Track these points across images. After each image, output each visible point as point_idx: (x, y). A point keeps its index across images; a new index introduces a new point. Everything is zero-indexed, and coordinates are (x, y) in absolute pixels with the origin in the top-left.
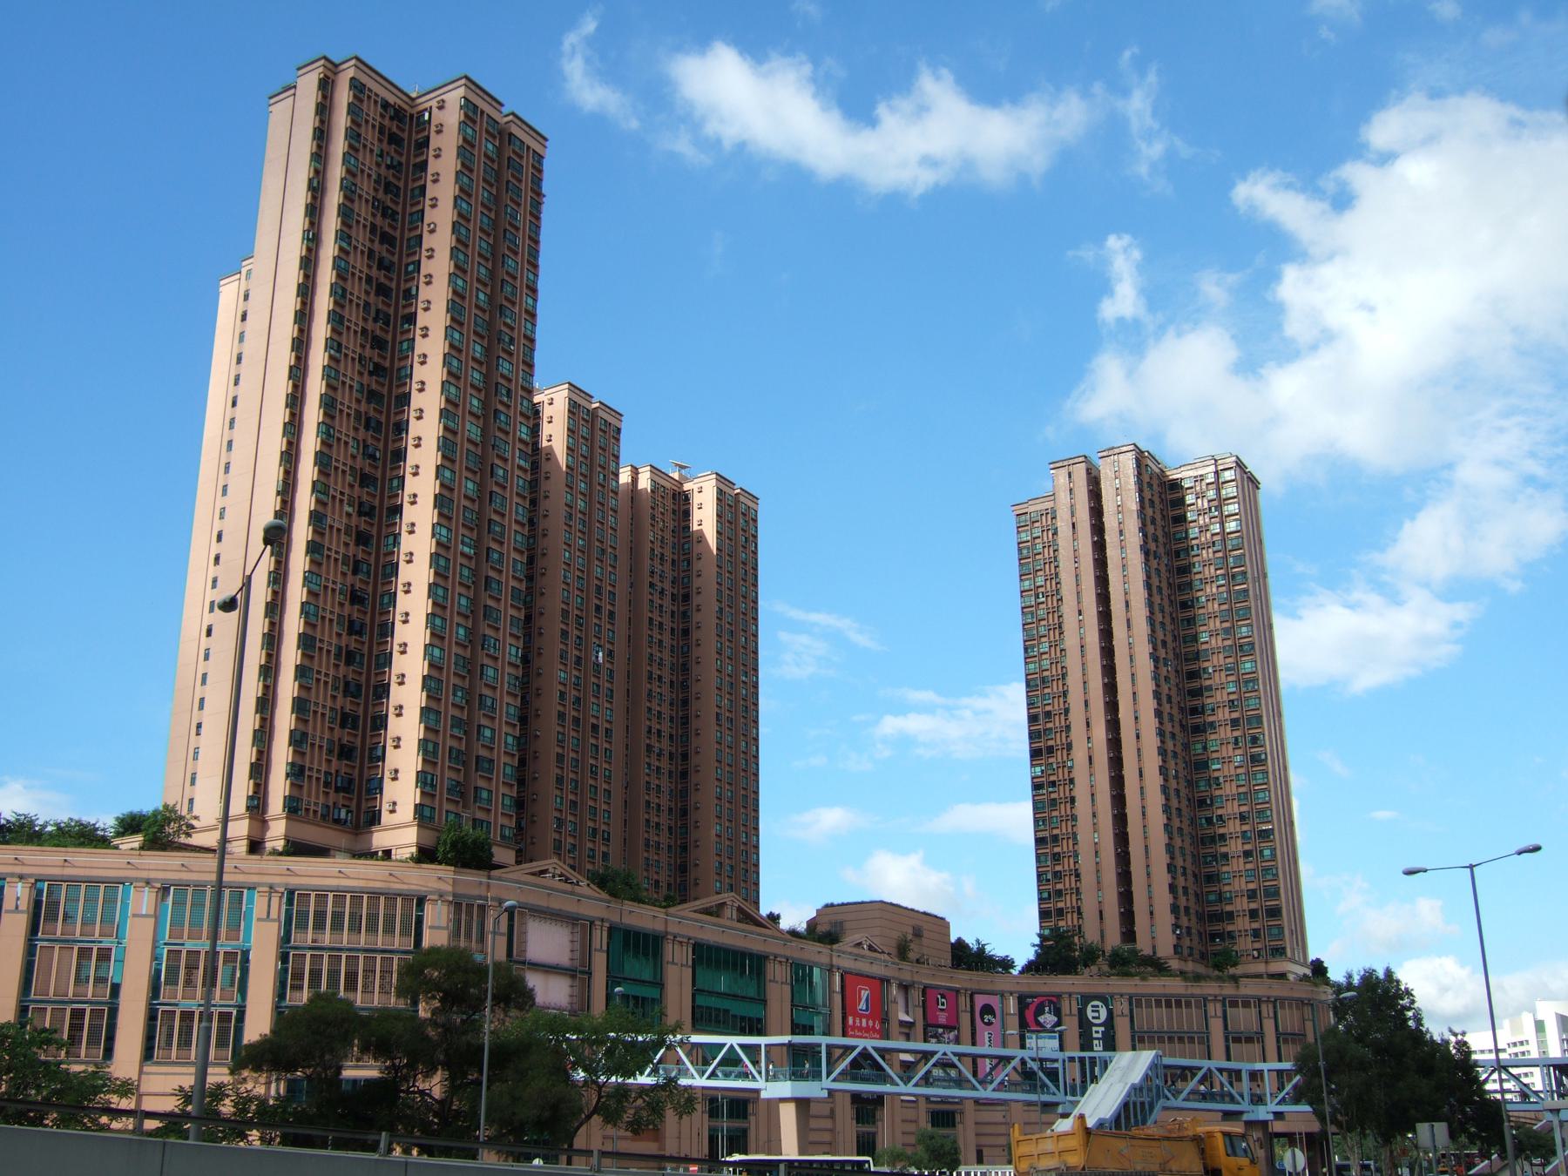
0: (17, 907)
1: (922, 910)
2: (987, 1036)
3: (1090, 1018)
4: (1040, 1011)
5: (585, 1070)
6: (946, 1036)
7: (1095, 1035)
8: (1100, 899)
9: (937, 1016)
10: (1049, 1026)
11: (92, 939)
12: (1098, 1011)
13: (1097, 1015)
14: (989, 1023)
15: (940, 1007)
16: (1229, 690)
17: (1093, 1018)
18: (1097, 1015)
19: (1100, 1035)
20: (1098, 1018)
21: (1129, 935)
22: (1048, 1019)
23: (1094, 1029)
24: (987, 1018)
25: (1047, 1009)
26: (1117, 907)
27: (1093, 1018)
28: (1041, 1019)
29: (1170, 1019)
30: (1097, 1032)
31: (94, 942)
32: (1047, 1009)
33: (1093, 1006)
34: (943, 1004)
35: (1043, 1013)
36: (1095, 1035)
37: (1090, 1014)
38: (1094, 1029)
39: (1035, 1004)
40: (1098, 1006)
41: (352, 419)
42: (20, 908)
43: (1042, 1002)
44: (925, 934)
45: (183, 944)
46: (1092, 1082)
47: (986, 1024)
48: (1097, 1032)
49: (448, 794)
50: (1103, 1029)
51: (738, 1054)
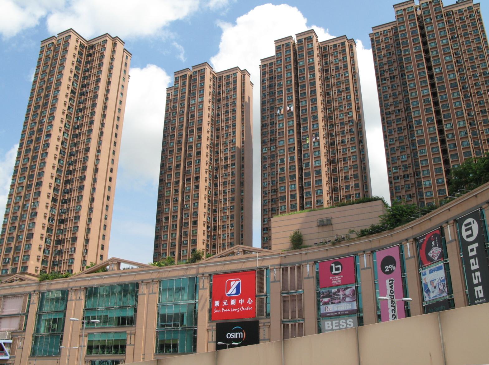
2: (388, 282)
3: (465, 238)
4: (429, 248)
6: (341, 293)
9: (331, 281)
10: (436, 258)
11: (287, 320)
14: (391, 271)
15: (334, 272)
16: (403, 160)
19: (475, 253)
20: (471, 235)
22: (436, 251)
24: (387, 268)
25: (433, 243)
30: (472, 250)
31: (289, 321)
32: (433, 243)
33: (466, 225)
37: (465, 234)
39: (425, 243)
40: (470, 224)
41: (84, 324)
44: (333, 221)
46: (292, 337)
48: (472, 250)
49: (465, 156)
50: (476, 245)
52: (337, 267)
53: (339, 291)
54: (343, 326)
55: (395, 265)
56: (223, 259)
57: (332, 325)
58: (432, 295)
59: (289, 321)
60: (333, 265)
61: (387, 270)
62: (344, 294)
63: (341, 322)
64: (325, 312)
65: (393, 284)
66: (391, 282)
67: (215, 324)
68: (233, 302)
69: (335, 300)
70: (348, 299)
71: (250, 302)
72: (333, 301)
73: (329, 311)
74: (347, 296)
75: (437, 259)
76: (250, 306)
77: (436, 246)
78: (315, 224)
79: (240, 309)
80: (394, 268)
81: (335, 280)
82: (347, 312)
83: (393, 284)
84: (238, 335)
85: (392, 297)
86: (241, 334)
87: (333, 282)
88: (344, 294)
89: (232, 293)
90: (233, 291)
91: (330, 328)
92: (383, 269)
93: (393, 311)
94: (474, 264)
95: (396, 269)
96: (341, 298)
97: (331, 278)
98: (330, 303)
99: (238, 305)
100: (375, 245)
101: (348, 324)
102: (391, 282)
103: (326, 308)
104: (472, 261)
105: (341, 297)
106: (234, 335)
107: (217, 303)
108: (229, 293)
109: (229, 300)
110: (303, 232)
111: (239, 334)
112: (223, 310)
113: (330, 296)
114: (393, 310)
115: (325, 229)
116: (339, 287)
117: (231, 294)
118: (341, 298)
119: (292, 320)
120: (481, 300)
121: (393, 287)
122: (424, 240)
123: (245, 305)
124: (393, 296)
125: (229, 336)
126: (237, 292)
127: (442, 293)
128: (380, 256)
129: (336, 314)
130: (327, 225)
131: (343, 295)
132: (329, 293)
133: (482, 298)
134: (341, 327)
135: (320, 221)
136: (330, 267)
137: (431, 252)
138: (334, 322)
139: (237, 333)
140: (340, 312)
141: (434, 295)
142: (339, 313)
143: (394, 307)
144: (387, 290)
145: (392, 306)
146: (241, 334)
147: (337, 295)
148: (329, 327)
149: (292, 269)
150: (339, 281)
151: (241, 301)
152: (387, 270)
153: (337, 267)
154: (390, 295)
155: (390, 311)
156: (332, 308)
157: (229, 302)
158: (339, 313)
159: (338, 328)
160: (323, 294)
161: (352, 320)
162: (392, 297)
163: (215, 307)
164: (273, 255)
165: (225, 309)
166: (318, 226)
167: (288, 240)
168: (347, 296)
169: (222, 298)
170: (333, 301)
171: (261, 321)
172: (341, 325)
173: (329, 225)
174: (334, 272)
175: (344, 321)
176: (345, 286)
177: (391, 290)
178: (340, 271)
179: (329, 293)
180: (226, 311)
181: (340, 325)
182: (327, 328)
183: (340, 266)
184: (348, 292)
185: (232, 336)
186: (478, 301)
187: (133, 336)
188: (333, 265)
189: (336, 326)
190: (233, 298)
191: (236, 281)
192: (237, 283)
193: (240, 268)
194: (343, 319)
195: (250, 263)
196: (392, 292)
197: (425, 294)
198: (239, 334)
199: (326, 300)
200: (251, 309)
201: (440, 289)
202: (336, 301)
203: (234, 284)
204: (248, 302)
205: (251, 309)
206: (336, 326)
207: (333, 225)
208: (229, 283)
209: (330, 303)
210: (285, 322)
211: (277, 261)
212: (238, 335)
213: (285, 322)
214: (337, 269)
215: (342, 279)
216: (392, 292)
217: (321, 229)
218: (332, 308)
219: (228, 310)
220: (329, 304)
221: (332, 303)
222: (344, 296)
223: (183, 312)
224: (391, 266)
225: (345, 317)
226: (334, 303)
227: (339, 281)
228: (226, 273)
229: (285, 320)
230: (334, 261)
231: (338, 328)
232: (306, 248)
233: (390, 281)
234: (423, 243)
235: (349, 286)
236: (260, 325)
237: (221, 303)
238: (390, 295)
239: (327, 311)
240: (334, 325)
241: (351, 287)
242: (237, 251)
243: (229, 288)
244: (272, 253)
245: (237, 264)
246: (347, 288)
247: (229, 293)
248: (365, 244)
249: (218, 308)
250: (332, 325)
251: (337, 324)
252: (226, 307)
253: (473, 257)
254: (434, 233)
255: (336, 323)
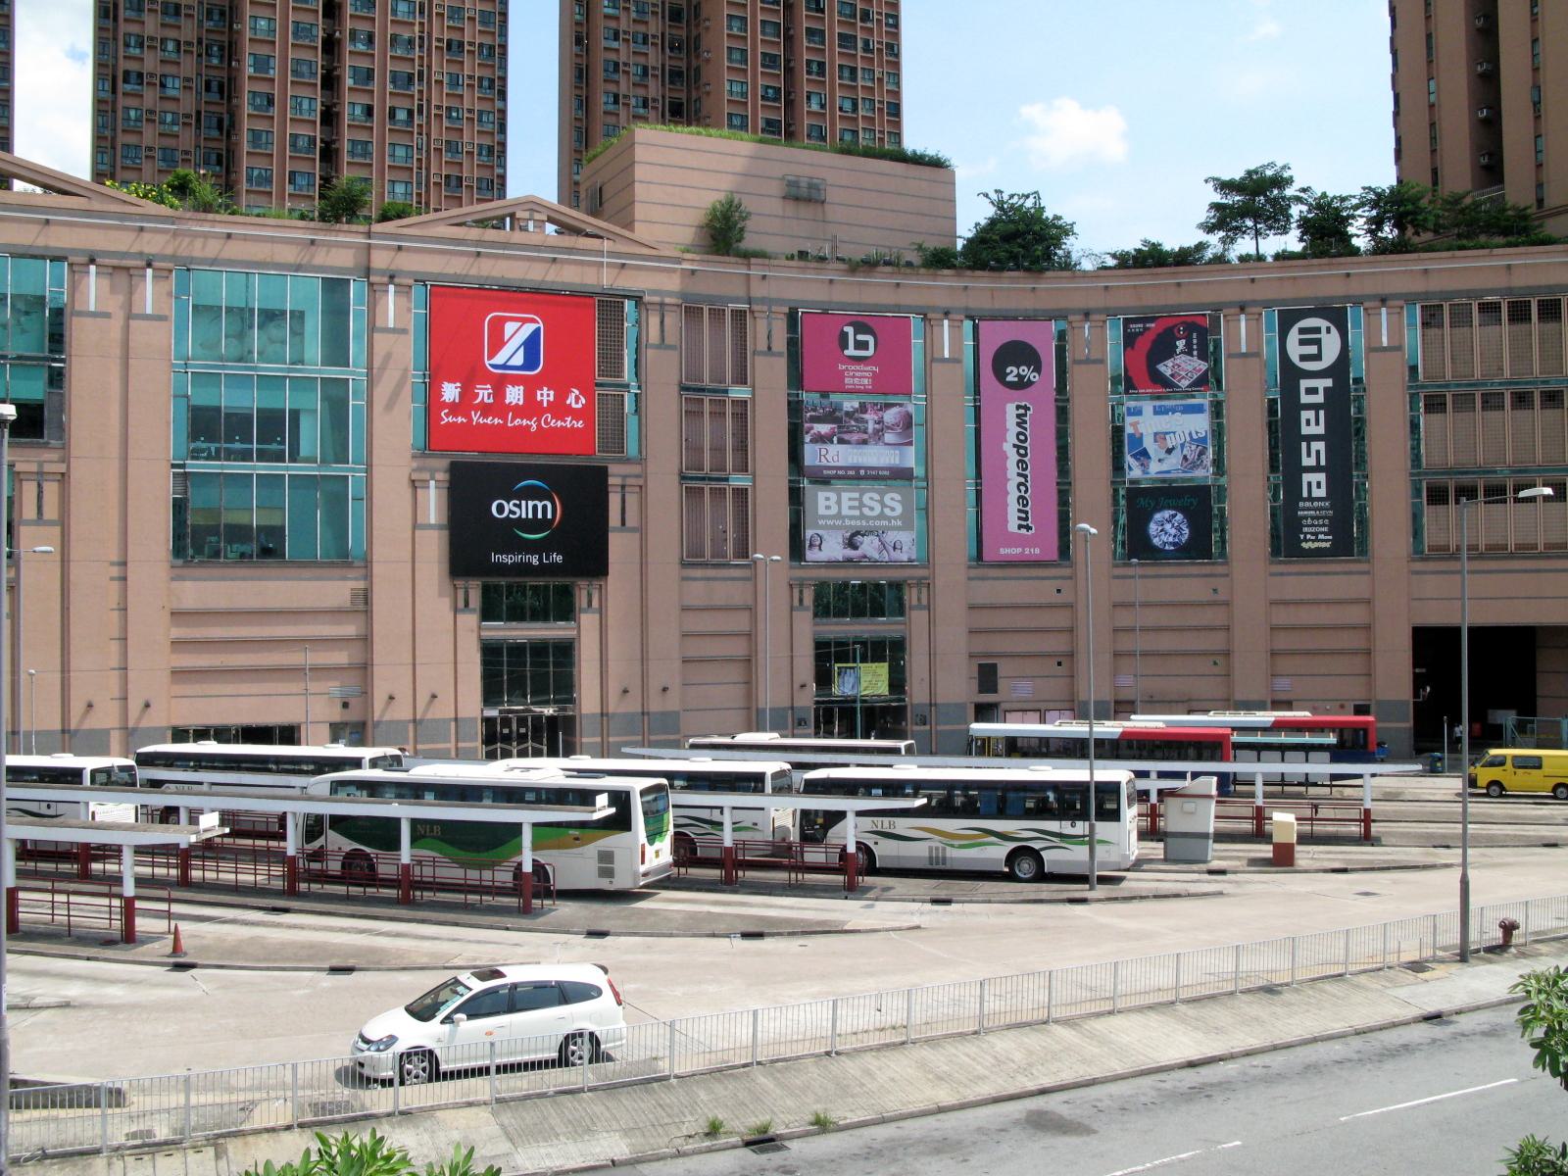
0: (769, 348)
1: (1393, 130)
2: (1011, 411)
3: (1295, 359)
4: (1163, 348)
5: (1030, 809)
6: (870, 417)
7: (1305, 399)
8: (1433, 98)
9: (841, 376)
10: (1184, 383)
12: (1318, 342)
13: (1313, 350)
14: (1022, 384)
15: (851, 351)
17: (1303, 358)
18: (1313, 350)
19: (1319, 398)
20: (1318, 357)
21: (1491, 169)
22: (1184, 366)
23: (1304, 384)
24: (1012, 373)
26: (780, 148)
27: (1303, 358)
28: (1166, 368)
29: (1520, 353)
30: (1312, 391)
31: (703, 479)
32: (1181, 344)
33: (1302, 331)
34: (861, 345)
35: (1170, 353)
36: (1305, 399)
38: (1304, 384)
40: (1317, 330)
42: (774, 349)
43: (1171, 329)
44: (832, 195)
45: (727, 480)
47: (1011, 386)
48: (1312, 391)
50: (1329, 382)
51: (429, 501)
52: (860, 337)
53: (863, 408)
54: (872, 509)
55: (1038, 369)
56: (474, 233)
57: (839, 502)
58: (1154, 468)
59: (703, 479)
60: (850, 330)
61: (1009, 378)
62: (880, 422)
63: (866, 499)
64: (817, 463)
65: (1027, 419)
66: (1022, 411)
67: (444, 463)
68: (514, 395)
69: (850, 432)
70: (889, 437)
71: (575, 400)
72: (846, 437)
73: (832, 464)
74: (888, 428)
75: (1189, 386)
76: (576, 414)
77: (1190, 353)
78: (776, 189)
79: (539, 421)
80: (1034, 377)
81: (854, 377)
82: (887, 473)
83: (1027, 419)
84: (535, 508)
85: (1022, 451)
86: (545, 508)
87: (847, 380)
88: (880, 422)
89: (510, 363)
90: (511, 353)
91: (834, 511)
92: (1000, 374)
93: (1023, 488)
94: (1313, 422)
95: (1045, 381)
96: (870, 430)
97: (842, 367)
98: (835, 439)
99: (531, 407)
100: (980, 302)
101: (887, 506)
102: (1022, 411)
103: (823, 452)
104: (1305, 415)
105: (871, 427)
106: (519, 506)
107: (450, 392)
108: (499, 359)
109: (499, 384)
110: (748, 204)
111: (540, 505)
112: (476, 418)
113: (837, 420)
114: (1020, 484)
115: (805, 211)
116: (869, 399)
117: (504, 367)
118: (870, 430)
119: (715, 474)
120: (1316, 504)
121: (1027, 426)
122: (1145, 329)
123: (559, 409)
124: (1025, 449)
125: (501, 509)
126: (531, 361)
127: (1192, 468)
128: (997, 335)
129: (851, 473)
130: (809, 200)
131: (876, 423)
132: (834, 411)
133: (1319, 499)
134: (866, 511)
135: (790, 184)
136: (838, 333)
137: (1169, 363)
138: (845, 496)
139: (531, 504)
140: (867, 468)
141: (1165, 467)
142: (862, 472)
143: (1025, 477)
144: (1006, 430)
145: (1019, 475)
146: (545, 508)
147: (856, 420)
148: (828, 508)
149: (717, 315)
150: (866, 381)
151: (545, 395)
152: (1009, 378)
153: (860, 337)
154: (1015, 446)
155: (1012, 487)
156: (837, 455)
157: (499, 392)
158: (862, 472)
159: (857, 513)
160: (815, 410)
161: (898, 497)
162: (1022, 451)
163: (445, 405)
164: (659, 259)
165: (485, 415)
166: (784, 198)
167: (698, 217)
168: (888, 428)
169: (472, 375)
170: (846, 437)
171: (613, 469)
172: (865, 506)
173: (816, 201)
174: (851, 351)
175: (877, 497)
176: (881, 399)
177: (1019, 434)
178: (870, 352)
179: (834, 411)
180: (489, 421)
181: (862, 505)
182: (822, 511)
183: (870, 339)
184: (890, 416)
185: (511, 512)
186: (1308, 504)
187: (51, 489)
188: (850, 330)
189: (850, 508)
190: (516, 381)
191: (525, 321)
192: (529, 328)
193: (539, 278)
194: (869, 491)
195: (573, 267)
196: (1022, 437)
197: (1129, 459)
198: (540, 505)
199: (823, 428)
200: (580, 424)
201: (1185, 458)
202: (855, 437)
203: (516, 333)
204: (571, 400)
205: (580, 424)
206: (850, 508)
207: (826, 206)
208: (497, 327)
209: (835, 439)
210: (692, 478)
211: (672, 283)
212: (535, 508)
213: (692, 478)
214: (861, 345)
215: (875, 377)
216: (1022, 437)
217: (790, 208)
218: (837, 455)
219: (496, 421)
220: (832, 442)
221: (841, 441)
222: (877, 426)
223: (296, 406)
224: (1024, 370)
225: (879, 486)
226: (848, 442)
227: (866, 381)
228: (505, 289)
229: (693, 473)
230: (854, 319)
231: (857, 513)
232: (766, 261)
233: (1018, 407)
234: (1141, 334)
235: (891, 400)
236: (611, 481)
237: (467, 393)
238: (1015, 446)
239: (824, 462)
240: (845, 504)
241: (901, 405)
242: (526, 215)
243: (498, 343)
244: (654, 252)
245: (527, 264)
246: (889, 406)
247: (499, 359)
248: (944, 288)
249: (454, 408)
250: (839, 502)
251: (856, 503)
252: (486, 410)
253: (1315, 407)
254: (1189, 320)
255: (850, 499)
